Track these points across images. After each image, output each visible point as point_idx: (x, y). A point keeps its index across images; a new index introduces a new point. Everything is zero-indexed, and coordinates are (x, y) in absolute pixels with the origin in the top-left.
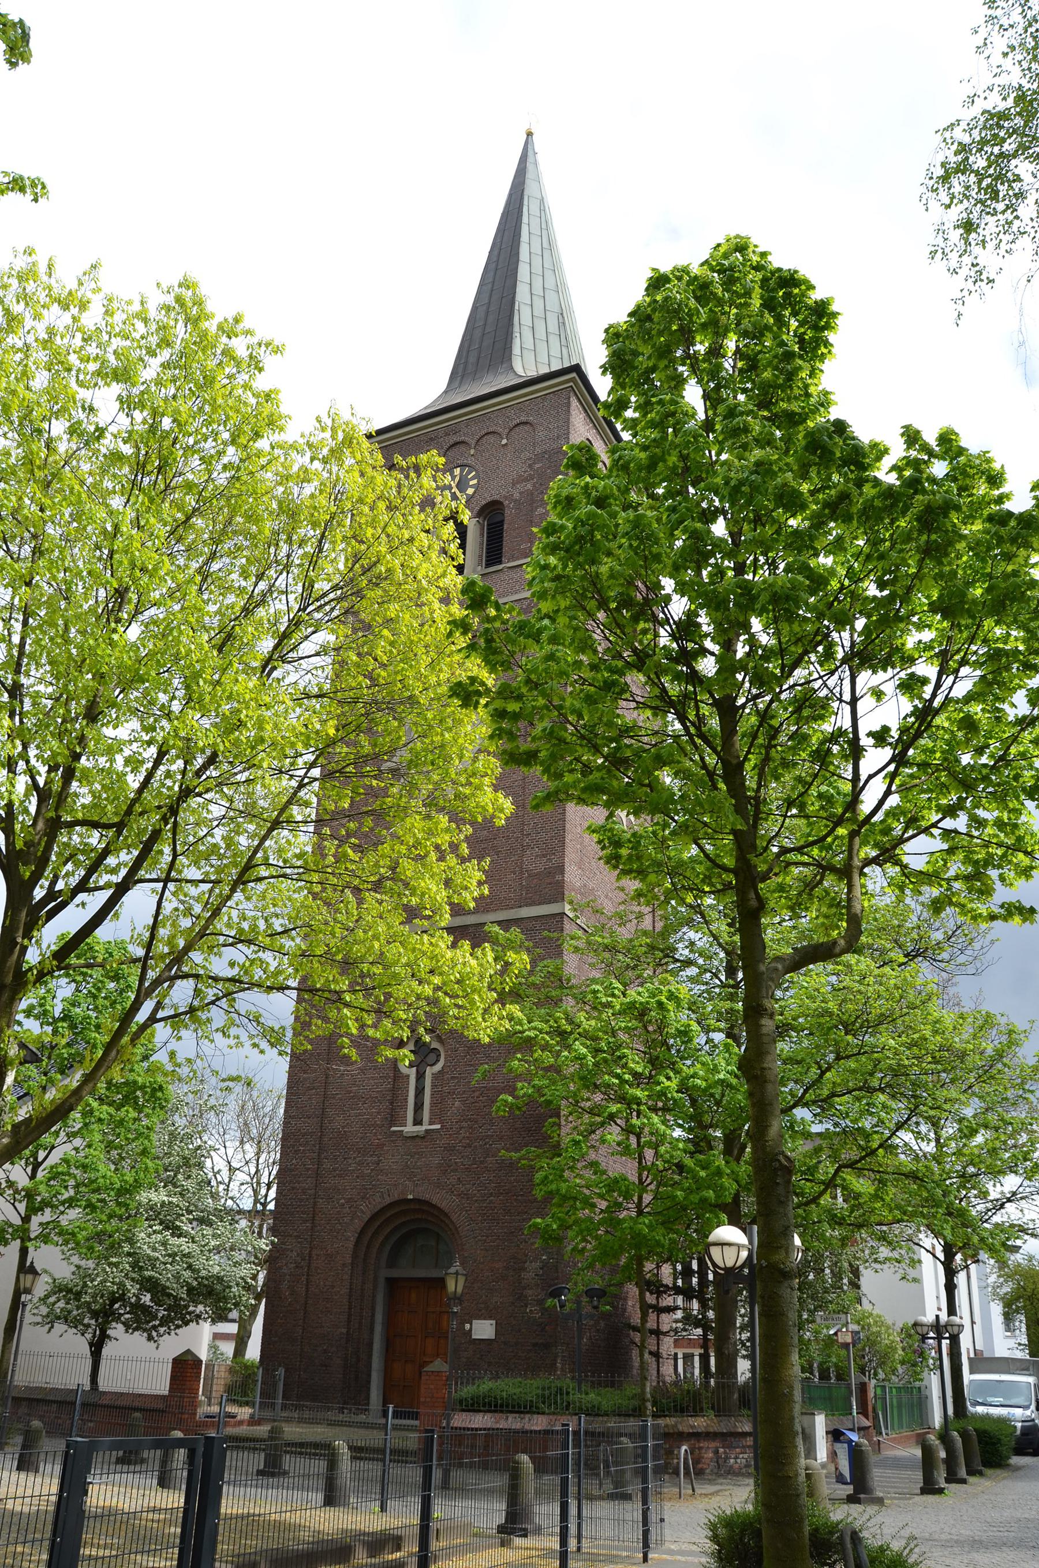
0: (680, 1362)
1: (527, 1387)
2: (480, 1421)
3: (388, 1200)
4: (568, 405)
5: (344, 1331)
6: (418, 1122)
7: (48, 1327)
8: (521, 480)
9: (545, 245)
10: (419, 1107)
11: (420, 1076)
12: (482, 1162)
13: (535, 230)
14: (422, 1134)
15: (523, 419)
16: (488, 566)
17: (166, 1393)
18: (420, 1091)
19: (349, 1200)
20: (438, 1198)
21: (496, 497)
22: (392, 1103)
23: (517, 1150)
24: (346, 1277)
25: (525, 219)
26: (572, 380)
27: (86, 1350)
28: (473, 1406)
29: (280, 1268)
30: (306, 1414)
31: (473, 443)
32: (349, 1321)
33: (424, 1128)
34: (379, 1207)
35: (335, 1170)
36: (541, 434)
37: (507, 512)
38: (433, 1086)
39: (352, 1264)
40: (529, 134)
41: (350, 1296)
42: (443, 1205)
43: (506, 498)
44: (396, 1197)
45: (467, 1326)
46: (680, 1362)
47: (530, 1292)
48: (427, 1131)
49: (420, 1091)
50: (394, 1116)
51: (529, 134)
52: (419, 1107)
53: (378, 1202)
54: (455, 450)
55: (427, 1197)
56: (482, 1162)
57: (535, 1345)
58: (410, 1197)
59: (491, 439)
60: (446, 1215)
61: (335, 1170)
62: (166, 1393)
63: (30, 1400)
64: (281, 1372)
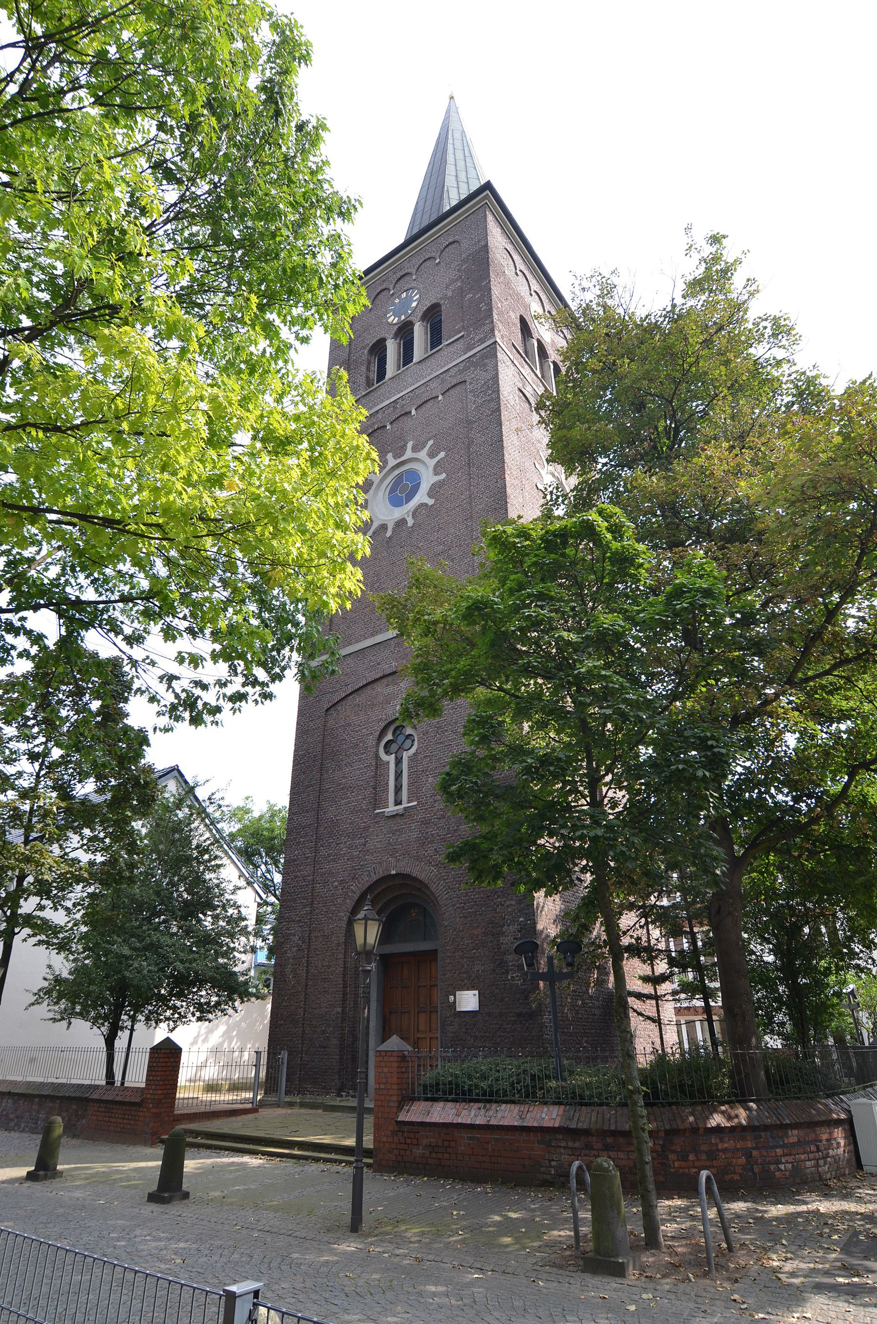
0: (684, 1027)
1: (508, 1067)
2: (442, 1113)
3: (375, 878)
4: (485, 216)
5: (340, 1010)
6: (398, 802)
7: (64, 1023)
8: (452, 282)
9: (467, 154)
10: (398, 789)
11: (398, 761)
12: (456, 831)
13: (458, 145)
14: (401, 812)
15: (451, 240)
16: (432, 348)
17: (143, 1085)
18: (398, 775)
19: (341, 882)
20: (421, 871)
21: (434, 301)
22: (375, 788)
23: (412, 759)
24: (341, 956)
25: (450, 141)
26: (487, 196)
27: (101, 1043)
28: (437, 1092)
29: (286, 952)
30: (308, 1099)
31: (414, 271)
32: (344, 1000)
33: (402, 807)
34: (367, 885)
35: (329, 855)
36: (465, 244)
37: (443, 307)
38: (410, 768)
39: (346, 943)
40: (452, 98)
41: (344, 975)
42: (422, 876)
43: (441, 299)
44: (381, 875)
45: (452, 998)
46: (684, 1027)
47: (510, 957)
48: (405, 808)
49: (398, 775)
50: (378, 800)
51: (452, 98)
52: (398, 789)
53: (367, 880)
54: (401, 281)
55: (407, 871)
56: (456, 831)
57: (519, 1015)
58: (393, 872)
59: (428, 263)
60: (426, 886)
61: (329, 855)
62: (143, 1085)
63: (41, 1096)
64: (284, 1055)
